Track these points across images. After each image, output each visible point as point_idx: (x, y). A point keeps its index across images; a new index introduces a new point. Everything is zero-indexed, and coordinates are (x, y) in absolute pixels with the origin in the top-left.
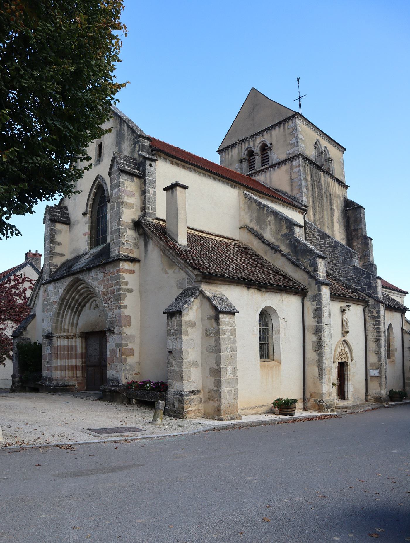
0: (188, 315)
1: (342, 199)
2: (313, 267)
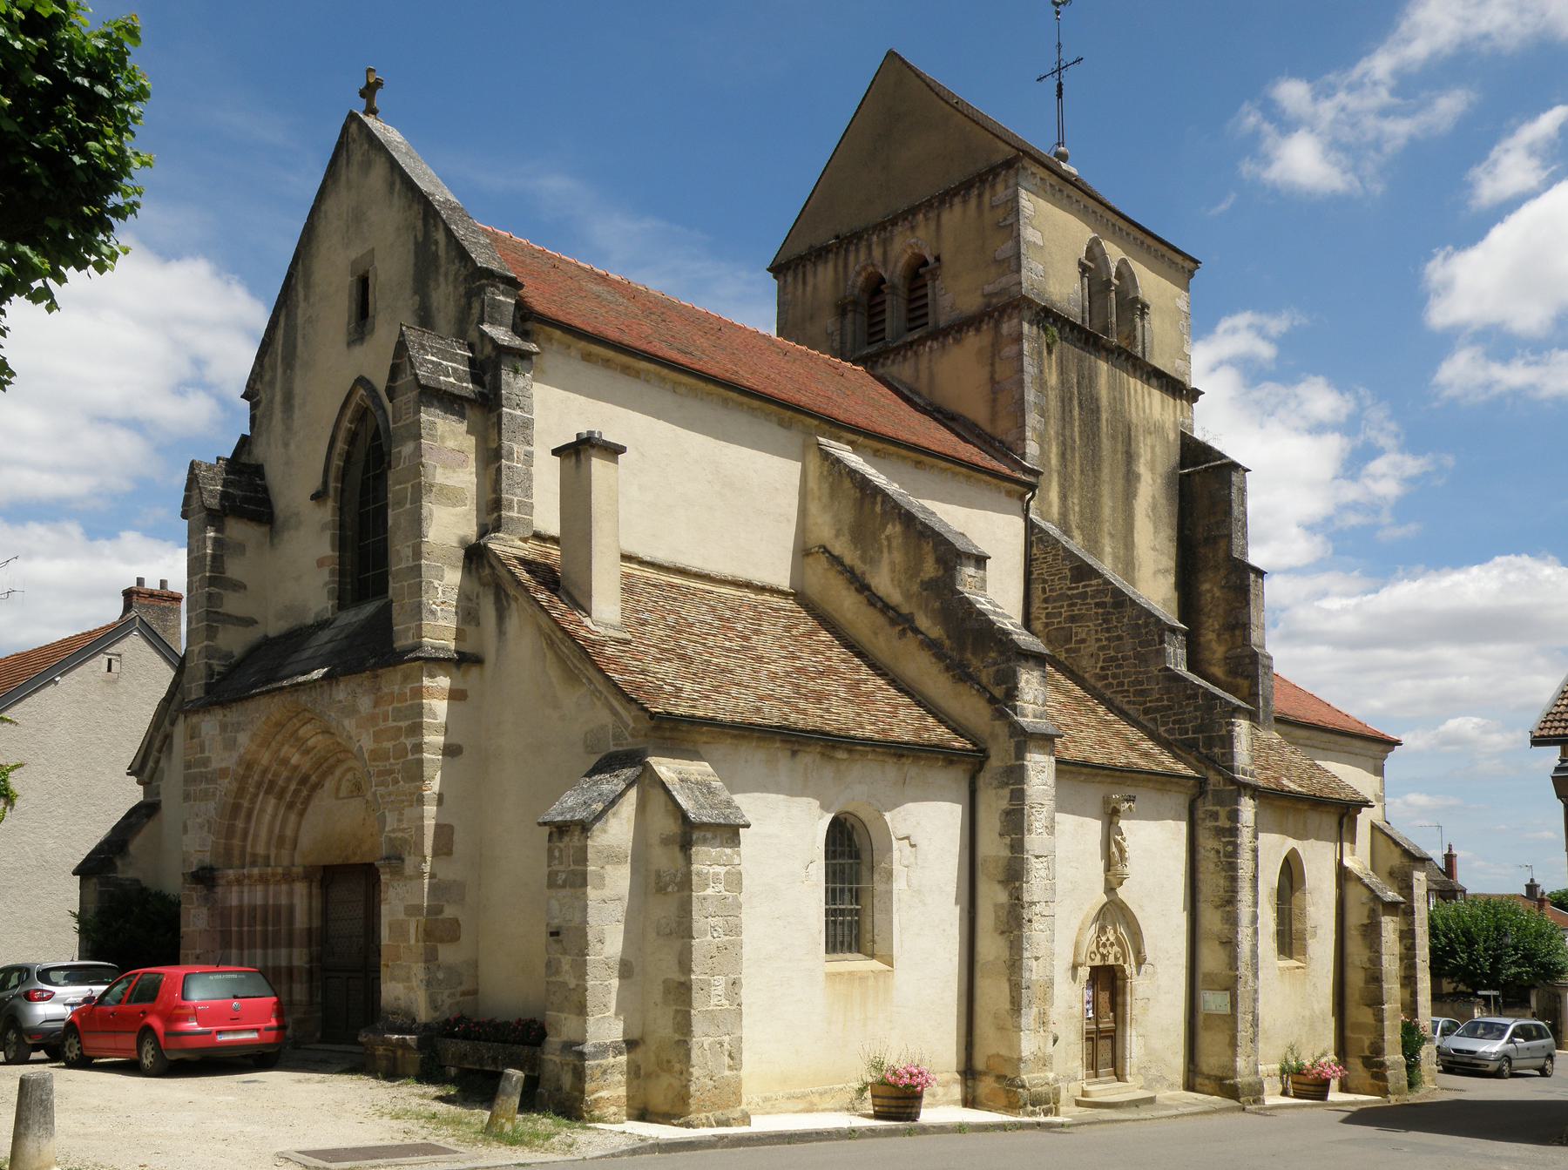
1: (1172, 436)
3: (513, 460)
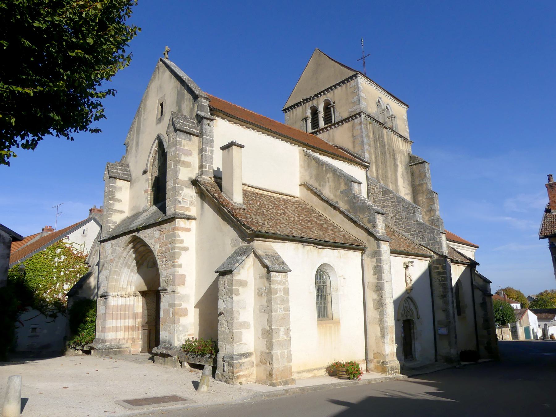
0: (239, 274)
1: (406, 154)
2: (371, 224)
3: (207, 152)
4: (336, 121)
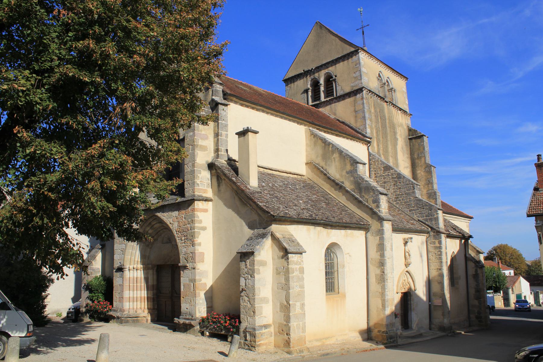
0: (259, 255)
4: (338, 95)
